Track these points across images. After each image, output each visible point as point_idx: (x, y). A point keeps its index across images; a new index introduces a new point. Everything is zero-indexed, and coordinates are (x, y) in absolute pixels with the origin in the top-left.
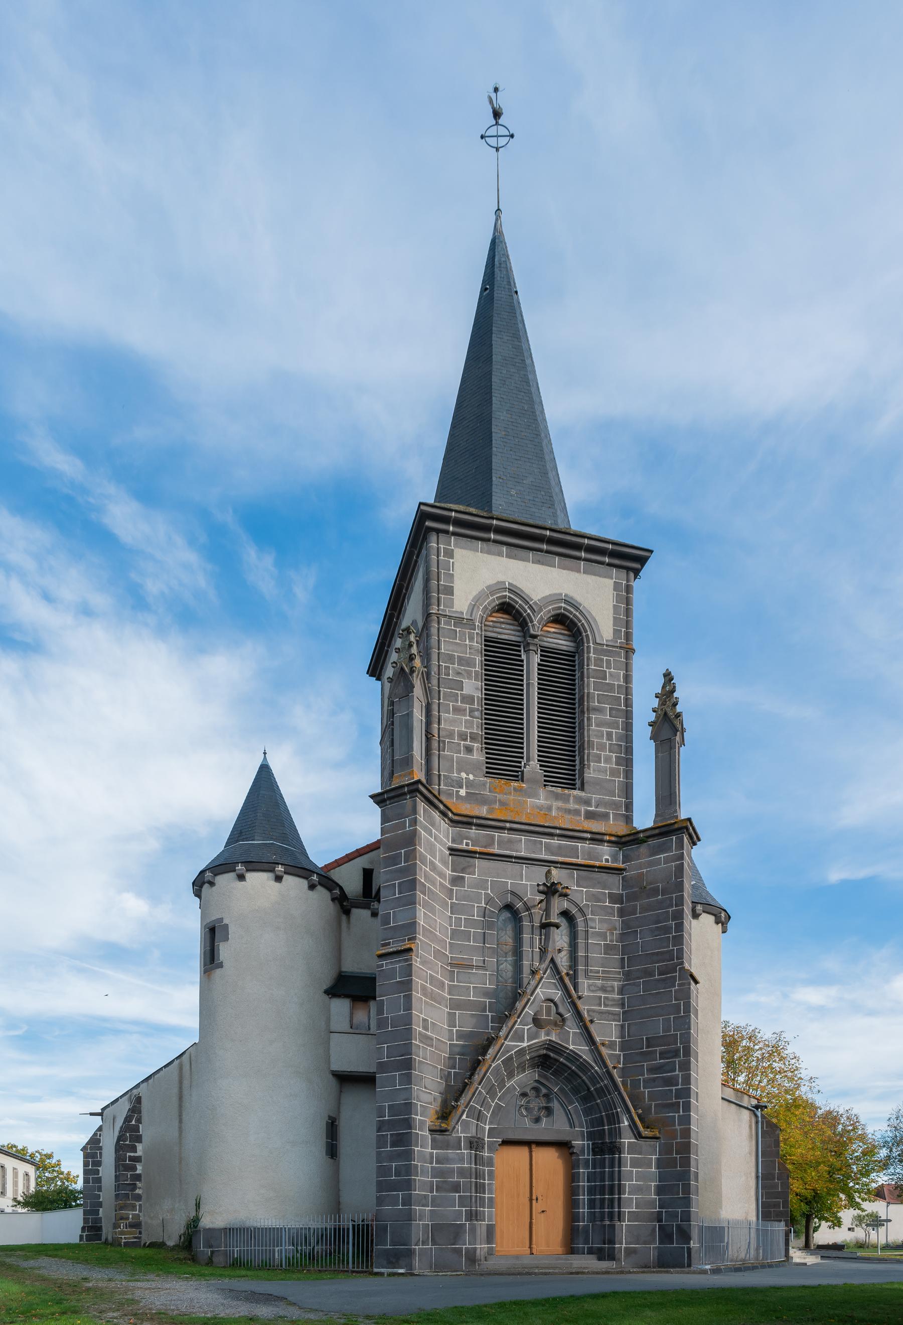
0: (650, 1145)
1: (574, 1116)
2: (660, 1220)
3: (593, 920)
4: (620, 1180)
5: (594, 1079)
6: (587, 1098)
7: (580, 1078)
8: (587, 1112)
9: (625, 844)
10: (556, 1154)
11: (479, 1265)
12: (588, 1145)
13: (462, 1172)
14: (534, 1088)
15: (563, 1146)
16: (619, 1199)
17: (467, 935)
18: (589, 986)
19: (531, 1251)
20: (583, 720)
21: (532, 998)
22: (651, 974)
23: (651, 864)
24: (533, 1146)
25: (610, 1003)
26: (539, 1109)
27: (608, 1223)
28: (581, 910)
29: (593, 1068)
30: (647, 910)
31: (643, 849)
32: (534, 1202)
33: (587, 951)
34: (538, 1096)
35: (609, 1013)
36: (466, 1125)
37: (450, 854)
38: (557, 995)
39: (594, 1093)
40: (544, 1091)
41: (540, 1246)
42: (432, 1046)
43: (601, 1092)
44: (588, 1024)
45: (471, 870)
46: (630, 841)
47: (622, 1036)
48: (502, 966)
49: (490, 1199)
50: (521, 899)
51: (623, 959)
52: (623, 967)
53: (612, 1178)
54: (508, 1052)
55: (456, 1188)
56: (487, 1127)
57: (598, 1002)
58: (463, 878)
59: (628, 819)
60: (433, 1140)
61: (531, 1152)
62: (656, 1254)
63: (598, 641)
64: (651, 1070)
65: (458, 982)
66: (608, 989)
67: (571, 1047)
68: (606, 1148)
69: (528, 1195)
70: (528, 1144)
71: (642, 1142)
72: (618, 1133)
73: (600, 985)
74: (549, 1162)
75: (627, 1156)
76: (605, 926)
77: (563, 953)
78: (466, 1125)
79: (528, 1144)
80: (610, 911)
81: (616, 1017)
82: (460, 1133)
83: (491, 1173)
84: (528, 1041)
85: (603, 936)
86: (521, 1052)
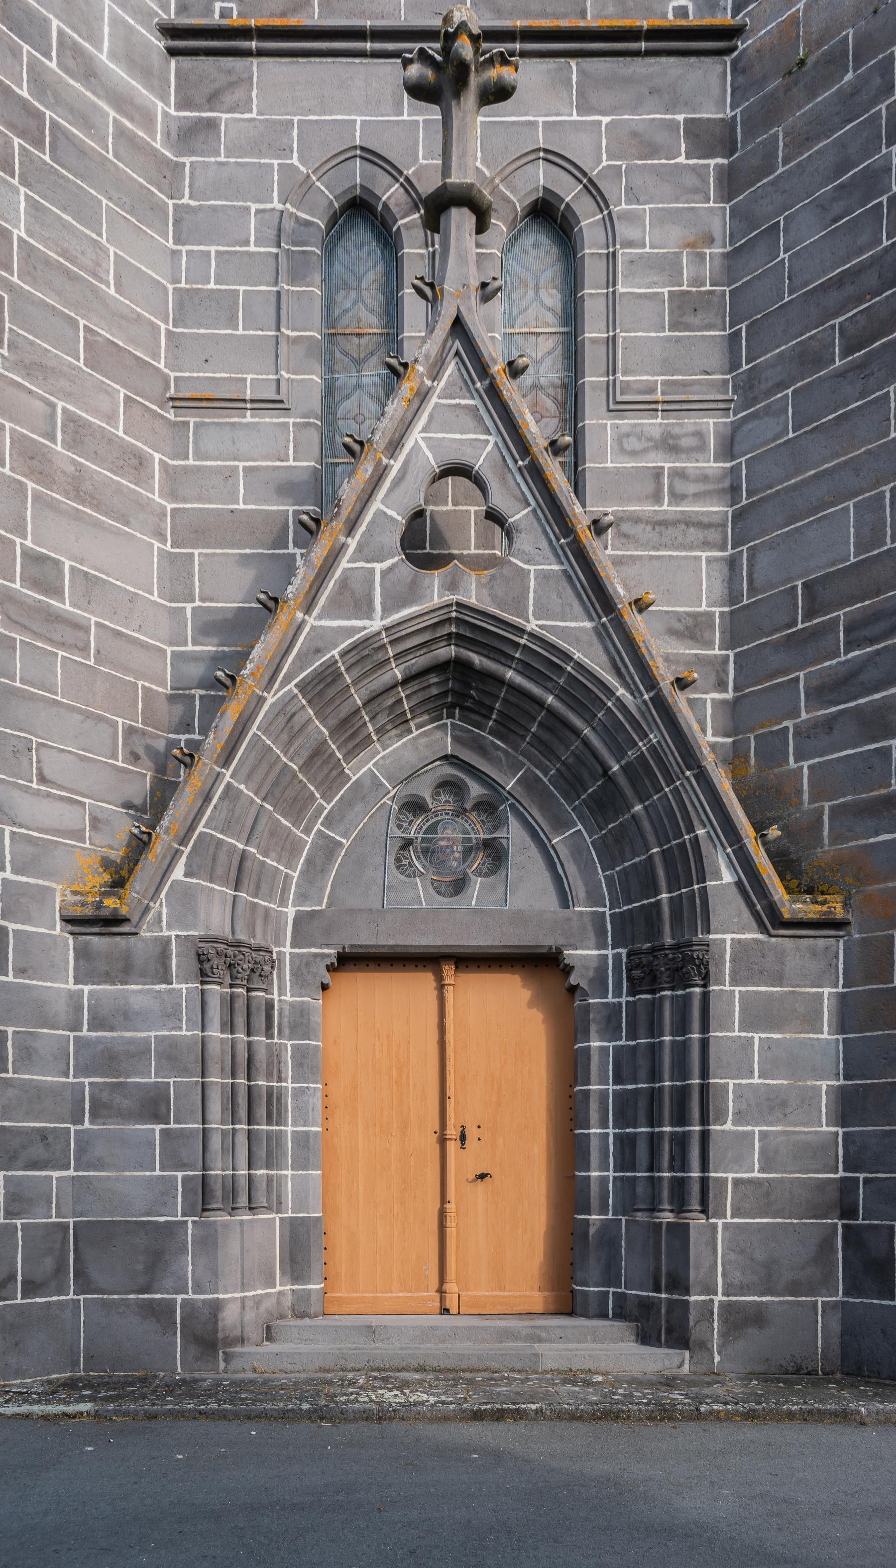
0: (814, 953)
1: (571, 869)
2: (848, 1212)
3: (631, 218)
4: (705, 1073)
5: (616, 736)
6: (605, 805)
7: (577, 733)
8: (611, 850)
10: (526, 994)
11: (228, 1358)
12: (617, 957)
13: (171, 1055)
14: (445, 785)
15: (540, 963)
16: (705, 1136)
17: (224, 307)
18: (620, 439)
19: (442, 1300)
21: (396, 466)
24: (448, 970)
25: (692, 488)
26: (467, 852)
27: (667, 1217)
28: (592, 188)
29: (610, 692)
30: (809, 140)
32: (452, 1147)
33: (612, 320)
34: (460, 812)
35: (688, 521)
36: (185, 898)
37: (173, 52)
38: (483, 448)
39: (623, 781)
40: (476, 790)
41: (473, 1285)
42: (84, 649)
43: (641, 775)
45: (238, 94)
47: (733, 597)
48: (347, 404)
49: (302, 1140)
50: (394, 171)
51: (734, 338)
53: (681, 1069)
54: (318, 651)
55: (154, 1106)
56: (291, 911)
57: (650, 487)
58: (211, 125)
60: (82, 953)
61: (441, 987)
62: (836, 1327)
64: (821, 693)
65: (198, 456)
66: (685, 442)
67: (532, 625)
68: (665, 964)
69: (434, 1124)
70: (428, 960)
71: (784, 943)
72: (695, 912)
73: (656, 433)
74: (503, 1018)
75: (730, 992)
76: (675, 234)
78: (185, 898)
79: (428, 960)
80: (690, 180)
81: (714, 535)
82: (163, 923)
83: (306, 1063)
84: (387, 611)
85: (668, 267)
86: (366, 653)
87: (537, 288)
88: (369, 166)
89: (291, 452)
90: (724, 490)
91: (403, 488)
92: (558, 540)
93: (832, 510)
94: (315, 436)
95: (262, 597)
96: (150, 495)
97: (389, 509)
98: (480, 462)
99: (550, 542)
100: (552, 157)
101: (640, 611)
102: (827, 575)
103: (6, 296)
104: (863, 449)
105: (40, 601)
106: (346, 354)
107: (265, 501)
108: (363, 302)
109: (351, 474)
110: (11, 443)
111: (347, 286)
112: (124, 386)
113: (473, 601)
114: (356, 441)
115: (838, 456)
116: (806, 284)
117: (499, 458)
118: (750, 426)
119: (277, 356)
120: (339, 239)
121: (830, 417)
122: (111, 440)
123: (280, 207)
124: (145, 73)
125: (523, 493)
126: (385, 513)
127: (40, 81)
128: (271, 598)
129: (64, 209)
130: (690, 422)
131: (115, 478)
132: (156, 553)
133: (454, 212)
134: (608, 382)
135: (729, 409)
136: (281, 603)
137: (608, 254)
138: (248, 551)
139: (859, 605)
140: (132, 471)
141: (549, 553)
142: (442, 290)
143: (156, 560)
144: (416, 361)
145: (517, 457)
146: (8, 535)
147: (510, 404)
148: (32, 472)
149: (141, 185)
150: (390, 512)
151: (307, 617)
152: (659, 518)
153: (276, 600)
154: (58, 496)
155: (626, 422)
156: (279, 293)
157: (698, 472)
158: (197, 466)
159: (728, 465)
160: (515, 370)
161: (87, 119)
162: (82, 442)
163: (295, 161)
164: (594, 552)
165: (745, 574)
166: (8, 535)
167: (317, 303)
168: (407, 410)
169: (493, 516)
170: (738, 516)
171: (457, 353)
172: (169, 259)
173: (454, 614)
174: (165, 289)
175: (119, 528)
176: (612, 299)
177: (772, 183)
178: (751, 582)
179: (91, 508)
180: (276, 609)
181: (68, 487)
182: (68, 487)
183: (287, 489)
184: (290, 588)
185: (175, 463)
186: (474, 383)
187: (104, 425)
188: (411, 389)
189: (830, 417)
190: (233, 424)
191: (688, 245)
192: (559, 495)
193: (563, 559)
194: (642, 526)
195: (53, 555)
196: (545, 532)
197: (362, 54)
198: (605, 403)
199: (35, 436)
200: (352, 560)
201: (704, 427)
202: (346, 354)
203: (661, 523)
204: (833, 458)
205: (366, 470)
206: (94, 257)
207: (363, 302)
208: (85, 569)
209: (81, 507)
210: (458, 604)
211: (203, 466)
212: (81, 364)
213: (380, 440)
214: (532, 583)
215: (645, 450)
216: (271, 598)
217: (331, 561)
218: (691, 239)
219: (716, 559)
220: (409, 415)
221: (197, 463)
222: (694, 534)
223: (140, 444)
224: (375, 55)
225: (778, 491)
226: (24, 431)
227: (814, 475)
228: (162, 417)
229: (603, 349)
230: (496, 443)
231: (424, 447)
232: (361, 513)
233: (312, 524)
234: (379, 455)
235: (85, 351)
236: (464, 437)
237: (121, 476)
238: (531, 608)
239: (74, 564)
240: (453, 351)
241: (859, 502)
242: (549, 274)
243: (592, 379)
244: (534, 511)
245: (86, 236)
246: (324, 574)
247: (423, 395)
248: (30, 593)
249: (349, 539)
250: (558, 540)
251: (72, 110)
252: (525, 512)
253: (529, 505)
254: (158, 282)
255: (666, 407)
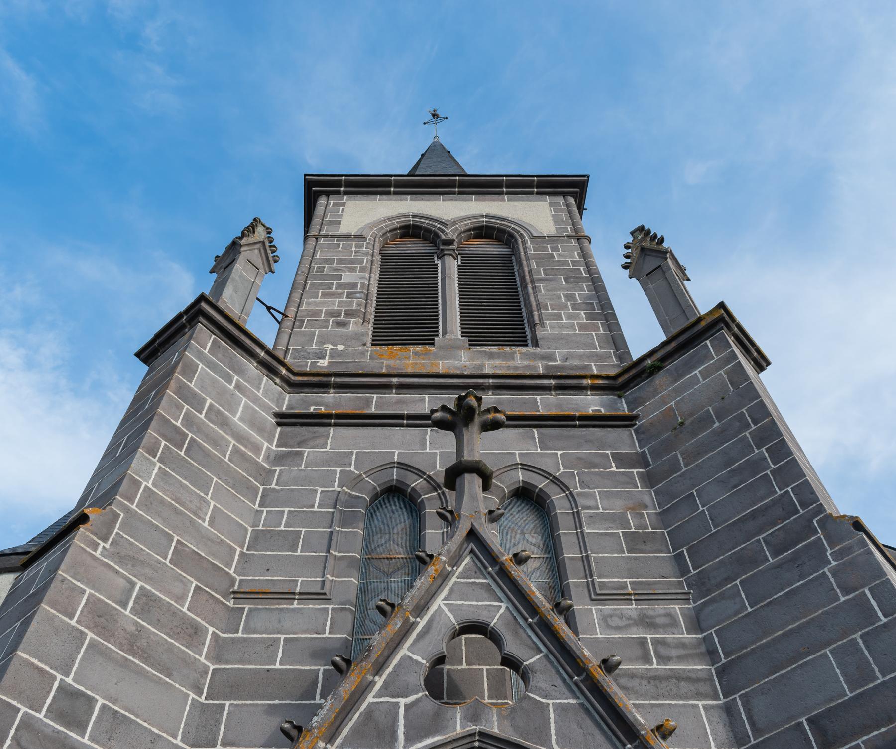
2: (646, 464)
9: (625, 387)
20: (527, 294)
21: (422, 623)
22: (756, 559)
23: (678, 392)
28: (556, 481)
31: (660, 379)
35: (678, 677)
37: (279, 424)
38: (497, 612)
44: (600, 675)
45: (319, 441)
46: (633, 376)
52: (684, 572)
57: (638, 652)
59: (617, 341)
63: (535, 234)
73: (634, 614)
77: (531, 565)
81: (704, 688)
87: (523, 534)
88: (403, 471)
89: (328, 628)
90: (702, 653)
91: (428, 638)
92: (572, 678)
93: (811, 657)
94: (350, 617)
95: (286, 725)
96: (197, 657)
97: (414, 654)
98: (495, 621)
99: (564, 681)
100: (525, 467)
101: (664, 737)
102: (829, 710)
103: (122, 515)
104: (820, 612)
105: (59, 732)
106: (379, 570)
107: (299, 663)
108: (393, 540)
109: (382, 627)
110: (86, 604)
111: (382, 532)
112: (197, 580)
113: (496, 730)
114: (388, 604)
115: (799, 619)
116: (726, 521)
117: (510, 617)
118: (711, 608)
119: (325, 567)
120: (378, 508)
121: (780, 594)
122: (175, 613)
123: (339, 489)
124: (261, 430)
125: (534, 643)
126: (411, 658)
127: (189, 421)
128: (295, 727)
129: (185, 478)
130: (659, 608)
131: (169, 640)
132: (189, 702)
133: (467, 477)
134: (588, 582)
135: (689, 599)
136: (304, 732)
137: (573, 513)
138: (277, 702)
139: (875, 733)
140: (186, 637)
141: (564, 690)
142: (459, 516)
143: (187, 708)
144: (439, 554)
145: (527, 616)
146: (52, 671)
147: (518, 579)
148: (96, 626)
149: (243, 476)
150: (415, 657)
151: (328, 746)
152: (651, 674)
153: (299, 729)
154: (112, 647)
155: (608, 608)
156: (331, 532)
157: (676, 641)
158: (244, 638)
159: (700, 636)
160: (519, 560)
161: (215, 442)
162: (149, 611)
163: (352, 468)
164: (608, 686)
165: (744, 718)
166: (52, 671)
167: (360, 539)
168: (431, 585)
169: (510, 662)
170: (721, 673)
171: (472, 551)
172: (253, 515)
173: (477, 744)
174: (246, 530)
175: (160, 679)
176: (582, 538)
177: (680, 476)
178: (753, 724)
179: (140, 660)
180: (298, 738)
181: (125, 642)
182: (125, 642)
183: (318, 653)
184: (315, 718)
185: (226, 635)
186: (486, 568)
187: (173, 602)
188: (436, 571)
189: (780, 594)
190: (282, 609)
191: (630, 509)
192: (569, 642)
193: (579, 694)
194: (637, 681)
195: (89, 693)
196: (558, 672)
197: (402, 425)
198: (587, 595)
199: (109, 602)
200: (378, 695)
201: (672, 611)
202: (379, 570)
203: (654, 678)
204: (795, 621)
205: (396, 623)
206: (198, 504)
207: (393, 540)
208: (116, 708)
209: (131, 658)
210: (481, 733)
211: (250, 638)
212: (167, 562)
213: (409, 602)
214: (552, 715)
215: (628, 626)
216: (295, 727)
217: (357, 696)
218: (631, 506)
219: (712, 707)
220: (433, 589)
221: (245, 636)
222: (684, 686)
223: (199, 619)
224: (408, 426)
225: (753, 649)
226: (101, 597)
227: (783, 634)
228: (223, 603)
229: (581, 563)
230: (507, 608)
231: (445, 609)
232: (388, 657)
233: (343, 665)
234: (408, 614)
235: (173, 554)
236: (480, 603)
237: (176, 640)
238: (554, 737)
239: (107, 703)
240: (469, 550)
241: (834, 649)
242: (531, 525)
243: (575, 581)
244: (546, 656)
245: (196, 493)
246: (349, 708)
247: (444, 577)
248: (52, 723)
249: (377, 678)
250: (572, 678)
251: (207, 436)
252: (538, 657)
253: (541, 652)
254: (242, 525)
255: (637, 597)
